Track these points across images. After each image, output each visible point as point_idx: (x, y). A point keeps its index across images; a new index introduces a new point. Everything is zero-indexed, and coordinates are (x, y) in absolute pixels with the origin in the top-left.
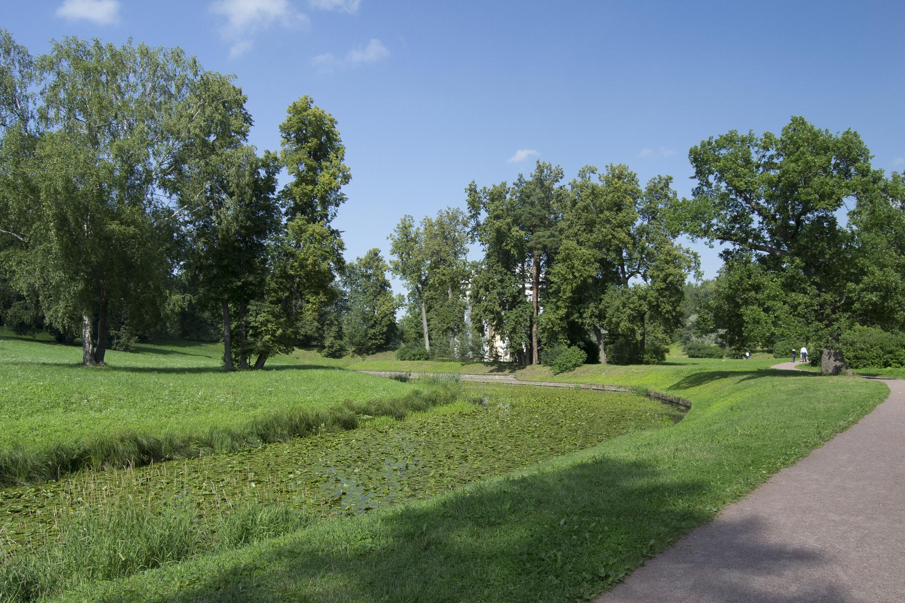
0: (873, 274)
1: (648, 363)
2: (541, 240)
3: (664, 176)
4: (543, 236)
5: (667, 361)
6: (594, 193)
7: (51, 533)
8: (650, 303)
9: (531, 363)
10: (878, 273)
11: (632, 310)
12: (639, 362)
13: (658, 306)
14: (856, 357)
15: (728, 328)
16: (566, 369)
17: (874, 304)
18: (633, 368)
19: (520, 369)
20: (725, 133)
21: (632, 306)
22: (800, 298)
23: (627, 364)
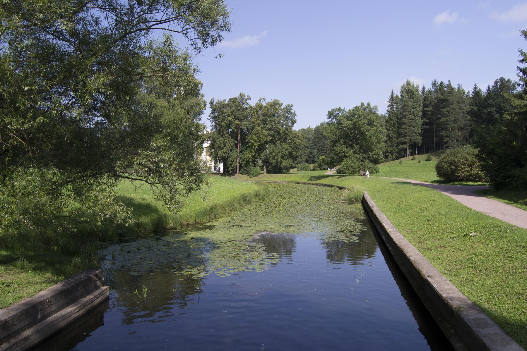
0: (376, 150)
1: (284, 173)
2: (246, 126)
3: (290, 104)
4: (247, 124)
5: (290, 173)
6: (261, 107)
7: (260, 206)
8: (289, 152)
9: (236, 173)
10: (377, 151)
11: (283, 154)
12: (281, 173)
13: (292, 153)
14: (354, 171)
15: (454, 175)
16: (255, 175)
17: (376, 158)
18: (279, 175)
19: (224, 176)
20: (338, 107)
21: (283, 153)
22: (358, 156)
23: (277, 173)
